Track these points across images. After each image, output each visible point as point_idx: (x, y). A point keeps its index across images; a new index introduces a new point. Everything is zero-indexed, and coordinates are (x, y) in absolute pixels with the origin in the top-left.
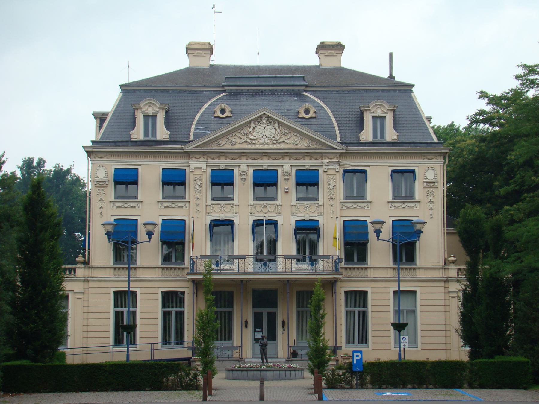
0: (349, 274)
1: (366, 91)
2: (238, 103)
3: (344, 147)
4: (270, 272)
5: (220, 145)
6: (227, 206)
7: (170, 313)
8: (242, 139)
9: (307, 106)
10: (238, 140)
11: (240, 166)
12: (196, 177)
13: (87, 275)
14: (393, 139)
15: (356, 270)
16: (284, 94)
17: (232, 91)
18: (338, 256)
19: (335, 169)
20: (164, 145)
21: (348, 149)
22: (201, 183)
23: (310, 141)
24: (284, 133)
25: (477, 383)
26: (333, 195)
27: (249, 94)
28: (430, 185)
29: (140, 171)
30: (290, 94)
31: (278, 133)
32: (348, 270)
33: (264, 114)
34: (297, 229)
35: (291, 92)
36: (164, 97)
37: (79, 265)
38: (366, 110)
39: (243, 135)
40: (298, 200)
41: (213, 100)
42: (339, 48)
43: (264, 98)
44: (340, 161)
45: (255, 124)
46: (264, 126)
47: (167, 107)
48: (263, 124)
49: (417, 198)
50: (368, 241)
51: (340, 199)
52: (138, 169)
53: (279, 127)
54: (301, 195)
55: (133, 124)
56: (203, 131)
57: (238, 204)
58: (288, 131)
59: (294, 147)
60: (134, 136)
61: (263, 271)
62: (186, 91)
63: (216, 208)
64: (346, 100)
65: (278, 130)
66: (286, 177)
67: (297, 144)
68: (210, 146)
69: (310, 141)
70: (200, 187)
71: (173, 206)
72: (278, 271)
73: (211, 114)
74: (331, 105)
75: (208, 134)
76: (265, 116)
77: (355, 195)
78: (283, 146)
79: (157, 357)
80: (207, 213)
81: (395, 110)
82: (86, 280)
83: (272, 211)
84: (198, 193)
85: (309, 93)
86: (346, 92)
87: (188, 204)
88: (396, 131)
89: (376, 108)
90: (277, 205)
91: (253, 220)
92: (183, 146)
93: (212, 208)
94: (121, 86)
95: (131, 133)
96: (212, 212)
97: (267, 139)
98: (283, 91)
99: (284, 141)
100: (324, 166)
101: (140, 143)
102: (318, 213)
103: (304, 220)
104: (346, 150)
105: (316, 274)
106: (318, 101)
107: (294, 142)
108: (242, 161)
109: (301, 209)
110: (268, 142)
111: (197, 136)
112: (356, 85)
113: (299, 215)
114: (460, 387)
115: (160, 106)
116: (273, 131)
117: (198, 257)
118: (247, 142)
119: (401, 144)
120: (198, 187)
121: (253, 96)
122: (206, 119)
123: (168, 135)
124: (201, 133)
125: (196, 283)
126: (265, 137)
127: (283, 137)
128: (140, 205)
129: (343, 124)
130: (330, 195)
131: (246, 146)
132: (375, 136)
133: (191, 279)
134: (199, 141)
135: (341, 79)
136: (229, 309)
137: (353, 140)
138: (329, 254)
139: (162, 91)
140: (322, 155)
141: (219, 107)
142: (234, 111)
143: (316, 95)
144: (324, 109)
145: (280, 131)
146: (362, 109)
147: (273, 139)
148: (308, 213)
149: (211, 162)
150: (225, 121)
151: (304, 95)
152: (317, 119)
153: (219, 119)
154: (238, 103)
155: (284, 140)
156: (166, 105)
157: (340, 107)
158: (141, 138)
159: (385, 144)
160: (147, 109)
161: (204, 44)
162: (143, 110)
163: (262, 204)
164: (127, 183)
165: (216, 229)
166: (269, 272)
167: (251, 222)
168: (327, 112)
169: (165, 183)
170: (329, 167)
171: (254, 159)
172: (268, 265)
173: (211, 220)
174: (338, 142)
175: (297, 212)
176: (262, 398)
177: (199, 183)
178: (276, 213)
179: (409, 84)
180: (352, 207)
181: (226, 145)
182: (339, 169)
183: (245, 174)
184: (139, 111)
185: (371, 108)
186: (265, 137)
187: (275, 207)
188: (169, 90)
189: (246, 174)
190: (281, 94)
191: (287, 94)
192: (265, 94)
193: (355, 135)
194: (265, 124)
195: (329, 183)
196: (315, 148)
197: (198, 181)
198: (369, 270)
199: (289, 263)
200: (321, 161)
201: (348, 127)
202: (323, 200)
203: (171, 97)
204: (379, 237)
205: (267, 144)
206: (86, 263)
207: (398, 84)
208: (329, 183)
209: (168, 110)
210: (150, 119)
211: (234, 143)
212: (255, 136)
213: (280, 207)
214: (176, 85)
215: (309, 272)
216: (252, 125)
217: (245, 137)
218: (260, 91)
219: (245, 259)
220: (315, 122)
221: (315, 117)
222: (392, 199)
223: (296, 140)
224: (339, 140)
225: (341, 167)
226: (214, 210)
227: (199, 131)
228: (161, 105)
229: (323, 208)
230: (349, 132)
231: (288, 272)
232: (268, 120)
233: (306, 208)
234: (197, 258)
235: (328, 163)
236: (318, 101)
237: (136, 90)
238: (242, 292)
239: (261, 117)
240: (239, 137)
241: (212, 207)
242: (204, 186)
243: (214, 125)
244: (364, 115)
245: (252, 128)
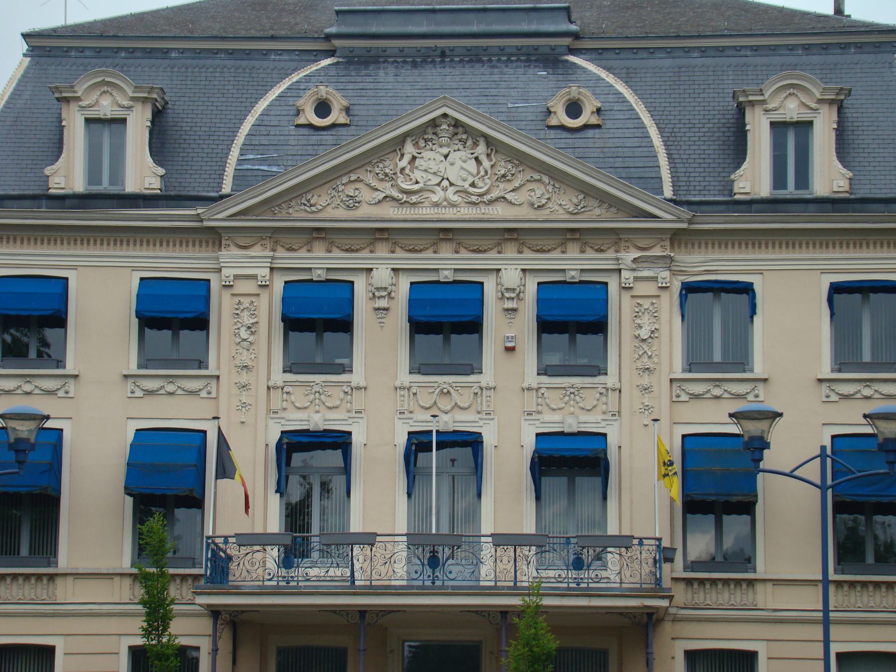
0: (701, 596)
1: (755, 49)
2: (371, 86)
3: (685, 213)
4: (447, 587)
5: (313, 209)
6: (331, 391)
8: (377, 190)
9: (574, 91)
10: (366, 195)
11: (371, 269)
12: (240, 303)
14: (835, 189)
15: (720, 586)
16: (509, 60)
17: (356, 53)
18: (659, 540)
19: (654, 279)
20: (146, 207)
21: (696, 219)
22: (255, 320)
23: (581, 197)
24: (502, 172)
26: (650, 357)
27: (405, 62)
29: (72, 284)
30: (525, 61)
31: (486, 172)
32: (696, 586)
33: (445, 115)
34: (540, 458)
35: (528, 55)
36: (154, 69)
38: (752, 104)
39: (382, 180)
40: (545, 374)
41: (295, 78)
43: (447, 70)
44: (672, 254)
45: (416, 145)
46: (445, 150)
47: (155, 96)
48: (441, 147)
50: (756, 496)
51: (671, 370)
52: (67, 279)
53: (488, 155)
54: (554, 359)
55: (57, 147)
56: (262, 168)
57: (362, 384)
58: (517, 166)
59: (531, 214)
60: (57, 180)
61: (428, 583)
62: (218, 51)
63: (299, 397)
64: (695, 78)
65: (486, 164)
66: (509, 305)
67: (543, 205)
68: (284, 212)
69: (581, 197)
70: (253, 333)
71: (170, 388)
72: (482, 584)
73: (286, 118)
74: (648, 92)
75: (273, 175)
76: (449, 120)
78: (499, 211)
80: (272, 412)
81: (842, 101)
83: (466, 405)
84: (245, 351)
85: (583, 56)
86: (695, 55)
87: (214, 383)
88: (844, 167)
89: (785, 95)
90: (481, 389)
91: (409, 433)
92: (199, 211)
93: (285, 395)
94: (25, 36)
95: (48, 171)
96: (285, 409)
97: (451, 190)
98: (507, 51)
99: (504, 198)
100: (623, 272)
101: (75, 201)
102: (604, 413)
103: (562, 434)
104: (690, 222)
105: (588, 593)
106: (610, 79)
107: (535, 198)
108: (378, 254)
109: (554, 399)
110: (455, 198)
111: (242, 180)
112: (725, 32)
113: (548, 417)
115: (134, 92)
116: (472, 166)
117: (231, 540)
118: (394, 199)
119: (858, 206)
120: (244, 334)
121: (415, 65)
122: (272, 133)
123: (159, 179)
124: (256, 173)
126: (445, 183)
127: (502, 186)
128: (71, 385)
129: (683, 148)
130: (642, 359)
131: (390, 211)
132: (779, 180)
133: (209, 606)
134: (248, 196)
135: (684, 19)
137: (712, 192)
138: (626, 532)
139: (149, 53)
141: (311, 96)
142: (356, 107)
143: (604, 63)
144: (625, 100)
145: (492, 166)
146: (741, 99)
147: (471, 190)
148: (572, 414)
149: (285, 258)
150: (327, 137)
151: (567, 61)
152: (604, 131)
153: (312, 132)
154: (371, 86)
155: (502, 194)
156: (152, 88)
157: (677, 96)
158: (79, 185)
159: (812, 206)
160: (97, 101)
162: (84, 103)
163: (436, 385)
165: (298, 459)
166: (443, 587)
167: (402, 440)
168: (634, 110)
170: (639, 274)
171: (416, 251)
172: (444, 565)
173: (282, 432)
174: (665, 199)
175: (540, 408)
177: (248, 321)
178: (479, 413)
179: (886, 26)
180: (708, 396)
181: (329, 209)
182: (668, 280)
183: (384, 293)
184: (74, 107)
185: (767, 95)
186: (445, 183)
187: (476, 394)
188: (169, 50)
189: (389, 294)
190: (499, 60)
191: (518, 60)
192: (452, 61)
193: (719, 179)
194: (448, 146)
195: (638, 321)
197: (246, 313)
198: (759, 587)
199: (505, 560)
200: (613, 255)
201: (697, 156)
202: (620, 374)
203: (176, 69)
204: (761, 463)
205: (453, 205)
207: (855, 27)
208: (638, 321)
209: (164, 108)
212: (417, 182)
213: (488, 393)
214: (189, 35)
215: (569, 589)
216: (409, 149)
217: (389, 185)
218: (438, 52)
219: (373, 545)
220: (597, 140)
221: (598, 126)
222: (832, 371)
223: (539, 192)
224: (668, 192)
225: (674, 273)
226: (293, 403)
227: (250, 167)
228: (137, 88)
229: (620, 397)
230: (702, 170)
231: (503, 588)
232: (456, 134)
233: (567, 398)
234: (226, 542)
235: (635, 260)
236: (607, 79)
237: (69, 49)
238: (361, 648)
239: (434, 124)
240: (368, 185)
241: (288, 393)
243: (297, 148)
244: (748, 118)
245: (407, 158)
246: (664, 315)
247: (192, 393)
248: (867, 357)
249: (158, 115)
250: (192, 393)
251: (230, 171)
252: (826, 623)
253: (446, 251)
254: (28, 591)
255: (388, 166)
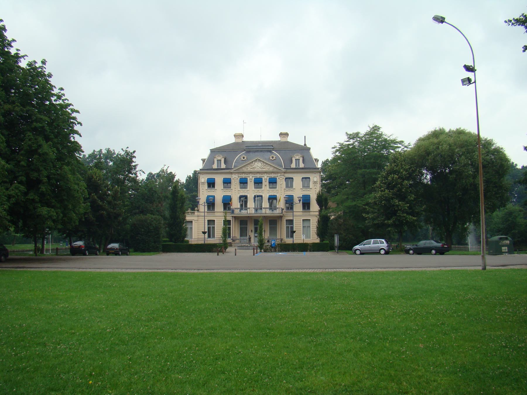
3: (285, 170)
7: (210, 227)
10: (249, 168)
13: (198, 214)
25: (312, 250)
28: (315, 183)
37: (196, 211)
42: (287, 134)
49: (311, 187)
54: (271, 187)
55: (214, 163)
59: (268, 170)
77: (289, 186)
78: (264, 170)
79: (206, 242)
82: (198, 216)
105: (274, 214)
106: (277, 154)
113: (241, 193)
114: (306, 251)
125: (235, 218)
131: (252, 170)
132: (296, 166)
136: (246, 226)
140: (278, 173)
161: (240, 134)
164: (273, 183)
169: (224, 183)
176: (236, 255)
196: (275, 170)
206: (198, 210)
210: (219, 161)
211: (247, 169)
216: (254, 163)
223: (269, 167)
224: (284, 167)
225: (284, 177)
242: (237, 184)
246: (283, 181)
247: (230, 191)
248: (289, 186)
249: (225, 159)
250: (230, 191)
251: (233, 166)
252: (293, 216)
253: (258, 174)
254: (307, 213)
255: (251, 165)
